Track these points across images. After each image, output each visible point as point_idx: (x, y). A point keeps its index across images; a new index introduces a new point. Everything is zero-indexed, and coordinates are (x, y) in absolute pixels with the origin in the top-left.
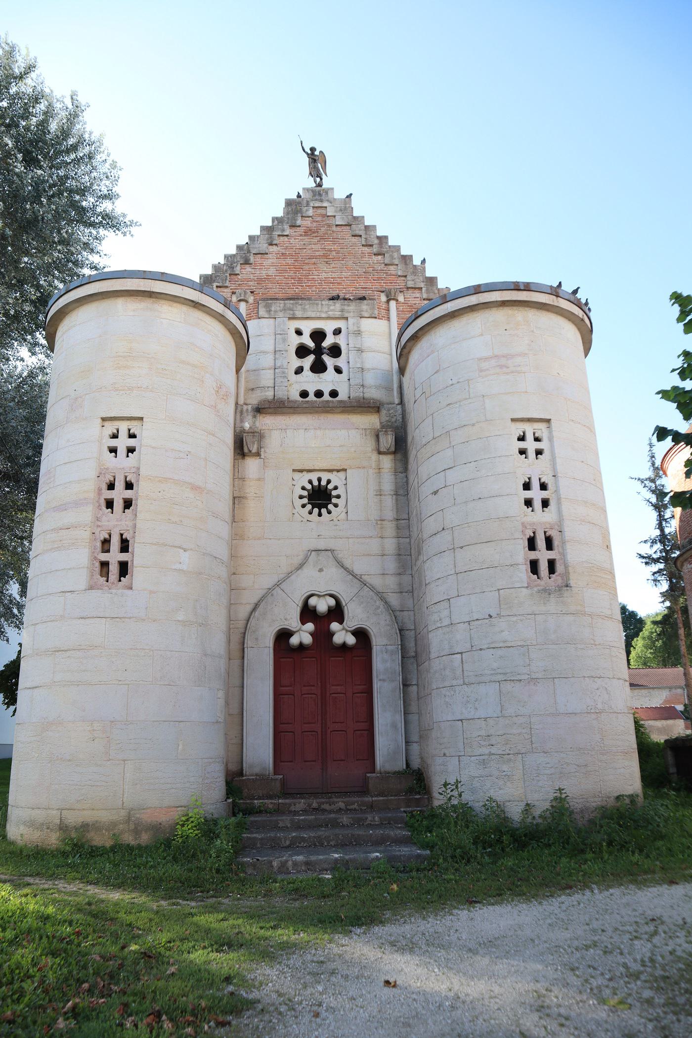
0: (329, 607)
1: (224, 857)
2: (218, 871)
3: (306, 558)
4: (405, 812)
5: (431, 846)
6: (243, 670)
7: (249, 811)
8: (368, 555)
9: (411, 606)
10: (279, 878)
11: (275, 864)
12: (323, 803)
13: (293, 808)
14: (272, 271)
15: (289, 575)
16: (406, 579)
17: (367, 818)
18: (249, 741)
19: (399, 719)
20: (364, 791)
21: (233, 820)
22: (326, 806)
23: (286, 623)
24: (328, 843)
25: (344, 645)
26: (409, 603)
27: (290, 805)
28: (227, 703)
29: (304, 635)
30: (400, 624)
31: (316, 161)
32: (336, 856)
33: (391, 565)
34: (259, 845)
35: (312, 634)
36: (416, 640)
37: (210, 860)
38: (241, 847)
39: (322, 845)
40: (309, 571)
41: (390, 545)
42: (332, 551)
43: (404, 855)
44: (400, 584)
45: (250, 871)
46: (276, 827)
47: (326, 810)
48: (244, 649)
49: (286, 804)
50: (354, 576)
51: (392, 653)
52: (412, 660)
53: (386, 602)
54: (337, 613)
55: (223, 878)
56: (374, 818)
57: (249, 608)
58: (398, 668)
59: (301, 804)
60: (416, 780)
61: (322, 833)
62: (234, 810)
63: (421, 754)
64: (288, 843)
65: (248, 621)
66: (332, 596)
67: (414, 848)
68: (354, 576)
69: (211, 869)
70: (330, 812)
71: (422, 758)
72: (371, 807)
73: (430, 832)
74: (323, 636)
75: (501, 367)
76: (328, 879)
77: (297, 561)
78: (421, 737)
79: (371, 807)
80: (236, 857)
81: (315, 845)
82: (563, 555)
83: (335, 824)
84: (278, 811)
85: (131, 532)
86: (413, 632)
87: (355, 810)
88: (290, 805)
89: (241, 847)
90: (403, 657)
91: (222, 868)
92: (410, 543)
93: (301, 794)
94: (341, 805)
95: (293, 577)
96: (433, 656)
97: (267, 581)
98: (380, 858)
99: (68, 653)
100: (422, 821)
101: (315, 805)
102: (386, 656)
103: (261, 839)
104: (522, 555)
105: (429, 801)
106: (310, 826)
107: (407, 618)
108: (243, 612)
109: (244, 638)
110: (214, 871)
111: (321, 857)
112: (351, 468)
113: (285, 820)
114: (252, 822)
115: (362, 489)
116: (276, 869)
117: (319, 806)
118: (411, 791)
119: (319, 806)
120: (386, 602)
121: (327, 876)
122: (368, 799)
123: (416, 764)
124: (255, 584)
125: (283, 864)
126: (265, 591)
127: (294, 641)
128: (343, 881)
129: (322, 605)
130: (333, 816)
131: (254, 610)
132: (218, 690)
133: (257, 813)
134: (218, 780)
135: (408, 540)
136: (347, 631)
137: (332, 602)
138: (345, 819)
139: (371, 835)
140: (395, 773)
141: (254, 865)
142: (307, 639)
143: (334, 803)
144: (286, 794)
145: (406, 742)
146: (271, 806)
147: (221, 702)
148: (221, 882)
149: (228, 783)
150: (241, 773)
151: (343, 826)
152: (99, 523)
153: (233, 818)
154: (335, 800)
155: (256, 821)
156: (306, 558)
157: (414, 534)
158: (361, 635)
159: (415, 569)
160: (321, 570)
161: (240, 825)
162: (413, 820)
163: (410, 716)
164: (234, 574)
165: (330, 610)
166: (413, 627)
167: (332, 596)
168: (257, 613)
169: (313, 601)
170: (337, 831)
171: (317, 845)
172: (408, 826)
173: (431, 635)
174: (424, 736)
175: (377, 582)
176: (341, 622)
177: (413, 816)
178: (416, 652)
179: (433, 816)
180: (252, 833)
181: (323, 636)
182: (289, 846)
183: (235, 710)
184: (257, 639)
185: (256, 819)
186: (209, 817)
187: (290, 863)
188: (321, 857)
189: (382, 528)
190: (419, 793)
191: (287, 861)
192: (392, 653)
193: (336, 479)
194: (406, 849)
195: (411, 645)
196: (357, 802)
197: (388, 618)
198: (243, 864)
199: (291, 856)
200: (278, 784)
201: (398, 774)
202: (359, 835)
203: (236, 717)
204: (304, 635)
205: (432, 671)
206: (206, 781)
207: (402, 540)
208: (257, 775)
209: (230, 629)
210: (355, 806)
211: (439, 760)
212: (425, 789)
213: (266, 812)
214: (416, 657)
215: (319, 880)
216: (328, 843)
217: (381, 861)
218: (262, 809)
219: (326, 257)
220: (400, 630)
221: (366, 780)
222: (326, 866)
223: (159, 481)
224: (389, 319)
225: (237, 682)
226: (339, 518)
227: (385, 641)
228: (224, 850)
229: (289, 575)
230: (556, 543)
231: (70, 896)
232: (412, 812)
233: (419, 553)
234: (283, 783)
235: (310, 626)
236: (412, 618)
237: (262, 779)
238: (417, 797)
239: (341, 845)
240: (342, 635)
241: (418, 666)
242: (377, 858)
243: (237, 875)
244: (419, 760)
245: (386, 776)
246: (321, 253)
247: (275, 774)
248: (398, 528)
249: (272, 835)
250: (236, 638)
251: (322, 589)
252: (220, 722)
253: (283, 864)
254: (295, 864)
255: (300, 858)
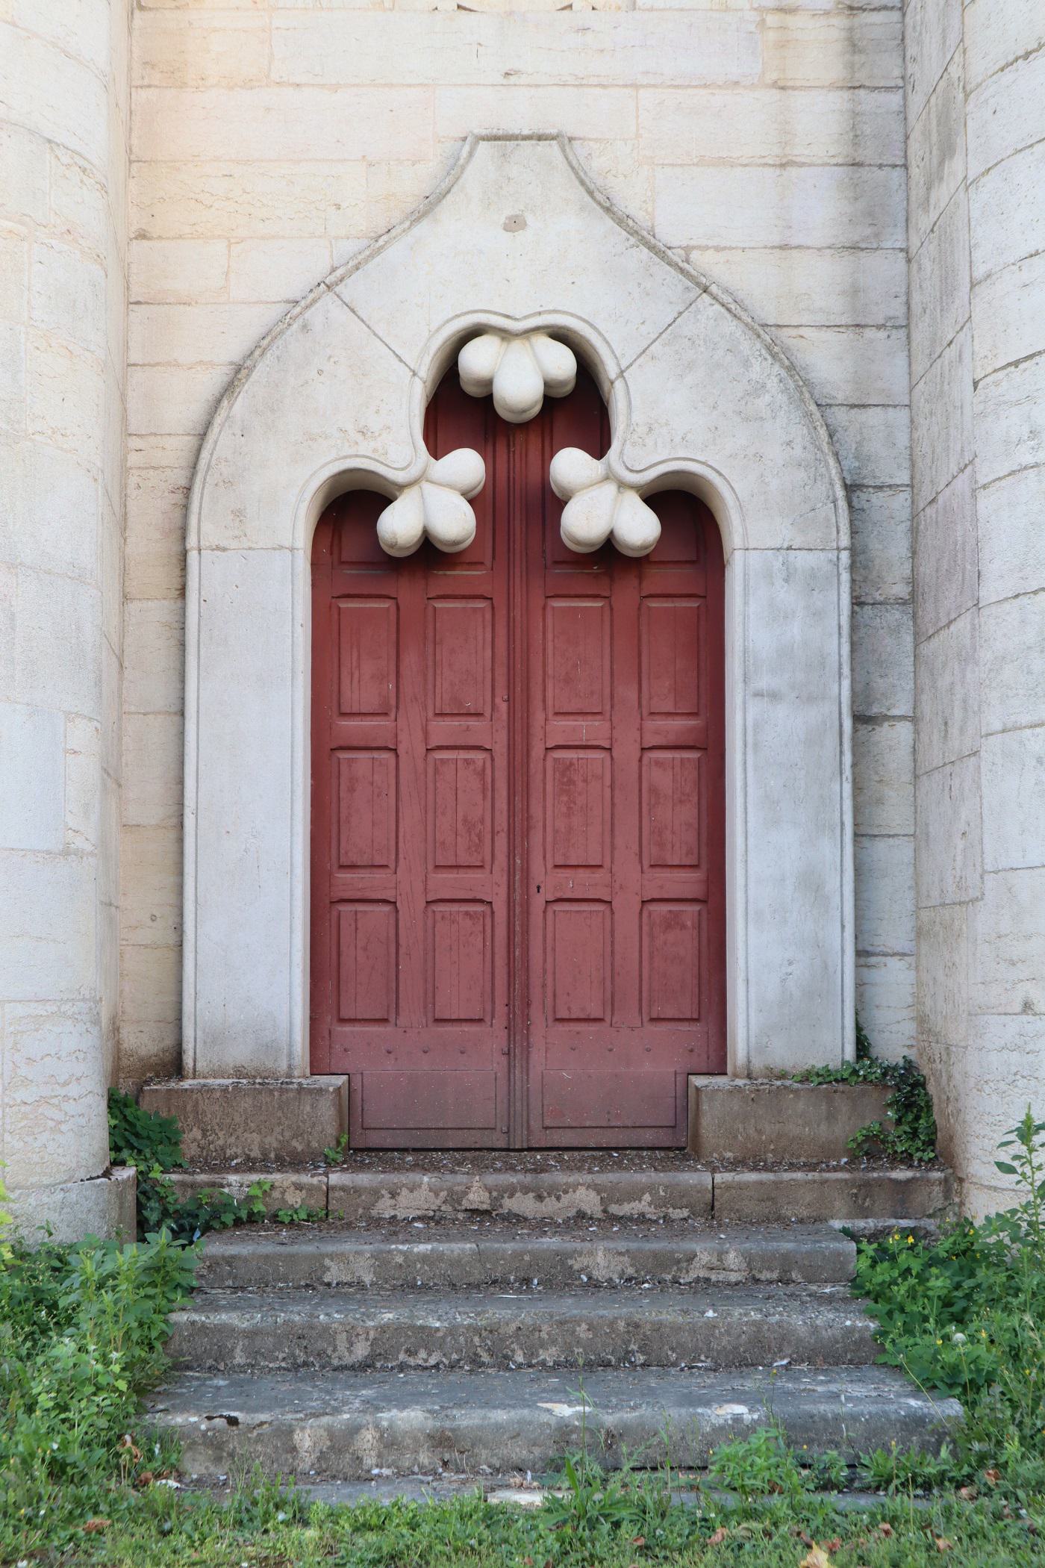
0: (547, 385)
1: (86, 1410)
2: (58, 1470)
3: (454, 171)
4: (849, 1234)
5: (967, 1384)
6: (182, 645)
7: (190, 1224)
8: (722, 162)
9: (899, 387)
10: (321, 1500)
11: (305, 1439)
12: (512, 1191)
13: (385, 1208)
15: (378, 241)
16: (883, 270)
17: (691, 1258)
18: (205, 935)
19: (834, 857)
20: (680, 1145)
21: (131, 1256)
22: (523, 1204)
23: (365, 447)
24: (531, 1353)
25: (608, 554)
26: (893, 374)
27: (375, 1194)
28: (113, 776)
30: (850, 463)
32: (564, 1411)
33: (820, 208)
34: (239, 1359)
36: (914, 531)
37: (25, 1425)
38: (159, 1369)
39: (503, 1362)
40: (464, 229)
41: (818, 120)
42: (563, 140)
43: (854, 1418)
44: (854, 292)
45: (195, 1469)
46: (314, 1285)
47: (519, 1219)
48: (184, 555)
49: (357, 1191)
50: (660, 252)
51: (812, 582)
52: (895, 615)
53: (791, 368)
54: (581, 409)
55: (78, 1502)
56: (721, 1255)
57: (210, 382)
58: (836, 647)
59: (418, 1192)
60: (901, 1111)
61: (506, 1312)
62: (145, 1213)
63: (918, 1001)
64: (361, 1351)
65: (203, 436)
66: (560, 335)
67: (893, 1387)
68: (660, 252)
69: (26, 1463)
70: (542, 1225)
71: (922, 1020)
72: (710, 1210)
73: (960, 1320)
74: (519, 507)
76: (530, 1514)
77: (413, 183)
78: (920, 933)
79: (710, 1210)
80: (140, 1410)
81: (476, 1362)
83: (560, 1278)
84: (323, 1218)
86: (904, 497)
87: (642, 1219)
88: (375, 1194)
89: (159, 1369)
90: (857, 602)
91: (76, 1454)
92: (903, 113)
93: (424, 1153)
94: (587, 1200)
95: (395, 252)
96: (990, 591)
97: (283, 270)
98: (752, 1428)
100: (922, 1279)
101: (477, 1197)
102: (786, 595)
103: (252, 1334)
105: (947, 1194)
106: (457, 1285)
107: (881, 438)
108: (181, 401)
109: (186, 507)
110: (40, 1471)
111: (500, 1416)
113: (352, 1257)
114: (213, 1264)
116: (306, 1461)
117: (496, 1202)
118: (871, 1149)
119: (496, 1202)
120: (791, 368)
121: (524, 1498)
122: (696, 1178)
123: (894, 1045)
124: (230, 284)
125: (341, 1442)
126: (282, 308)
127: (398, 525)
128: (593, 1524)
130: (550, 1242)
131: (229, 389)
132: (70, 716)
133: (238, 1223)
134: (74, 1090)
135: (895, 99)
136: (622, 485)
137: (562, 364)
138: (602, 1258)
139: (712, 1326)
140: (806, 1078)
141: (215, 1445)
142: (455, 522)
143: (556, 1192)
144: (357, 1152)
145: (861, 953)
146: (294, 1198)
147: (84, 770)
148: (70, 1519)
149: (115, 1104)
150: (174, 1065)
151: (594, 1284)
153: (132, 1249)
154: (561, 1178)
155: (230, 1260)
156: (454, 171)
157: (927, 71)
158: (683, 504)
159: (923, 221)
160: (515, 224)
161: (159, 1276)
162: (884, 1273)
163: (880, 850)
164: (142, 236)
165: (553, 402)
166: (903, 478)
167: (560, 335)
168: (239, 406)
169: (476, 360)
170: (568, 1306)
171: (486, 1359)
172: (860, 1289)
173: (986, 503)
174: (936, 927)
175: (756, 281)
176: (598, 443)
177: (884, 1255)
178: (913, 582)
179: (967, 1256)
180: (213, 1306)
181: (519, 507)
182: (365, 1366)
183: (152, 812)
184: (239, 514)
185: (232, 1250)
186: (34, 1239)
187: (368, 1438)
188: (500, 1416)
189: (782, 45)
190: (907, 1160)
191: (354, 1430)
192: (812, 582)
194: (858, 1390)
195: (891, 551)
196: (651, 1188)
197: (799, 433)
198: (167, 1438)
199: (373, 1406)
200: (327, 1112)
201: (824, 1081)
202: (658, 1327)
203: (159, 840)
205: (985, 655)
206: (21, 1095)
207: (869, 100)
208: (239, 1072)
209: (125, 470)
210: (642, 1206)
211: (1001, 1030)
212: (931, 1143)
213: (275, 1219)
214: (912, 601)
215: (491, 1517)
216: (531, 1353)
217: (758, 1440)
218: (259, 1207)
220: (851, 489)
221: (686, 1108)
222: (518, 1452)
225: (157, 692)
227: (783, 532)
228: (92, 1380)
229: (378, 241)
231: (522, 926)
232: (874, 1236)
233: (947, 150)
234: (349, 1106)
235: (467, 465)
236: (902, 439)
237: (259, 1087)
238: (901, 1174)
239: (590, 1365)
240: (600, 502)
241: (920, 637)
242: (739, 1430)
243: (139, 1484)
244: (909, 1028)
245: (773, 1086)
247: (316, 1069)
248: (853, 46)
249: (296, 1315)
250: (151, 511)
251: (519, 301)
252: (79, 854)
253: (341, 1442)
254: (390, 1442)
255: (411, 1418)
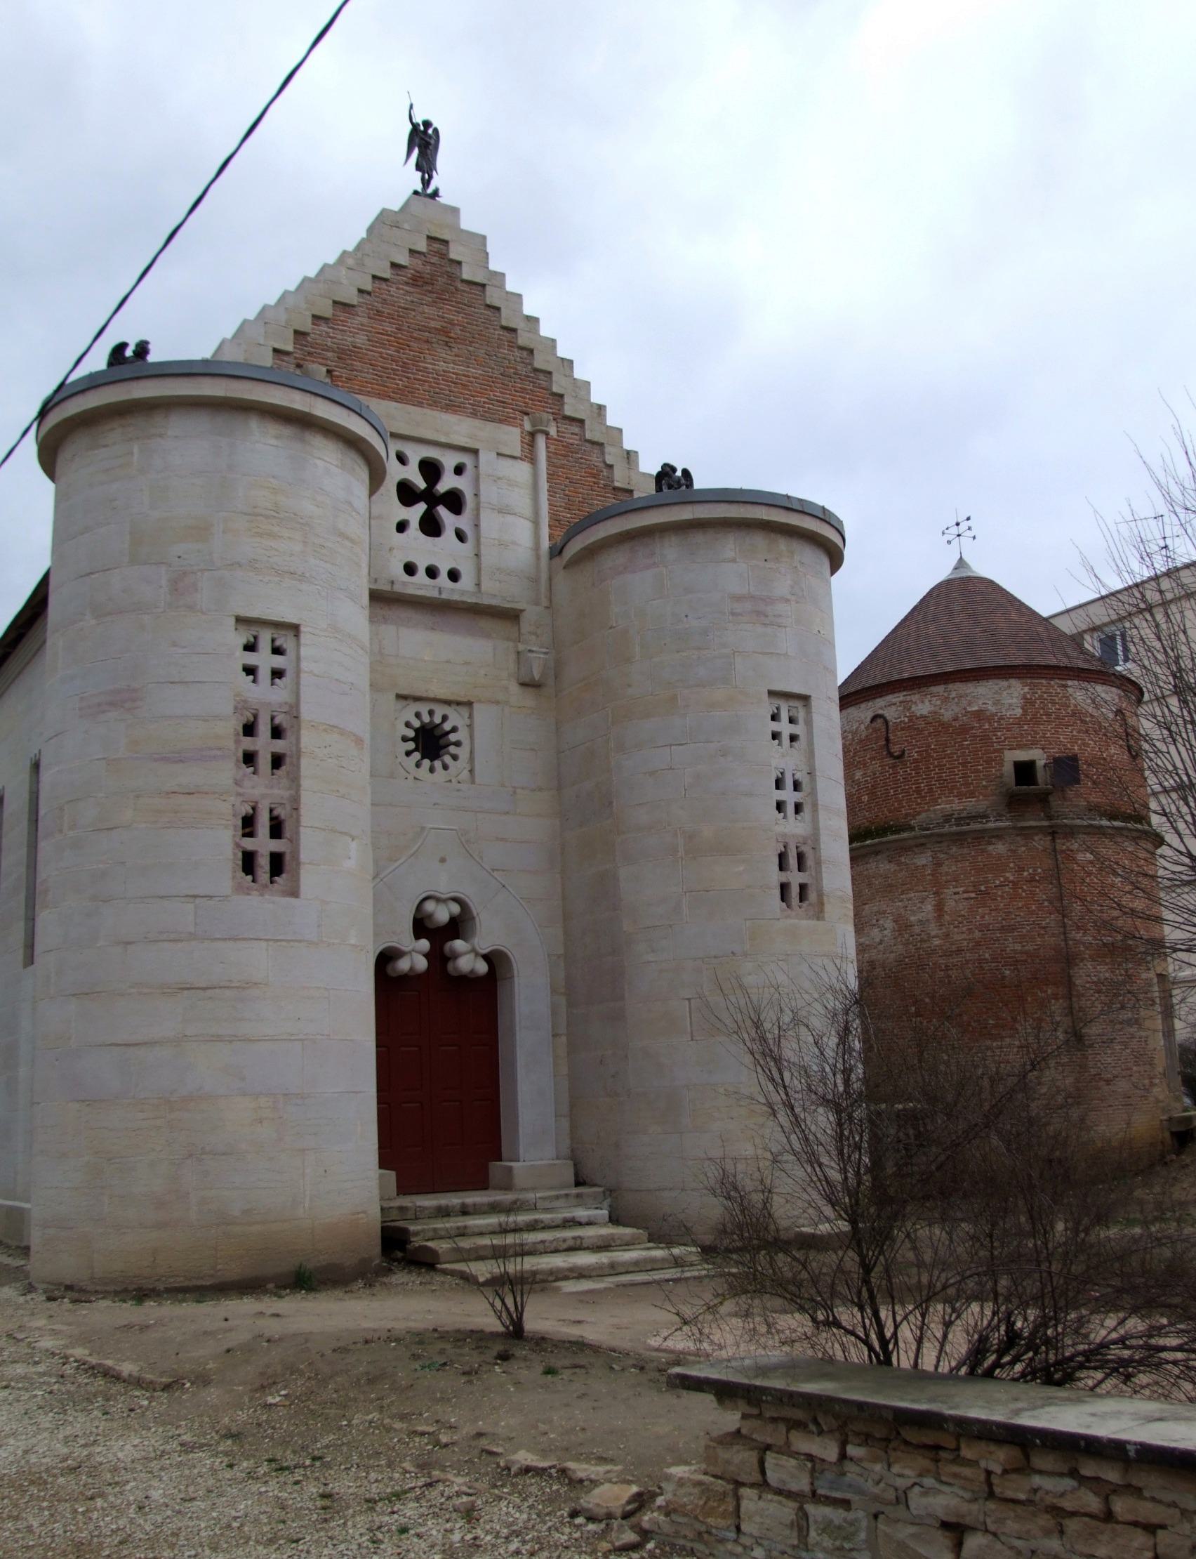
14: (361, 340)
29: (415, 958)
31: (423, 141)
35: (426, 956)
66: (455, 900)
74: (439, 958)
75: (759, 613)
82: (818, 878)
85: (288, 807)
99: (209, 993)
104: (775, 877)
112: (479, 701)
115: (496, 738)
127: (403, 965)
129: (442, 914)
137: (456, 909)
152: (241, 790)
167: (455, 900)
169: (430, 906)
181: (439, 958)
193: (456, 718)
204: (415, 958)
219: (446, 335)
223: (325, 730)
224: (533, 460)
226: (460, 778)
230: (810, 862)
246: (437, 325)
